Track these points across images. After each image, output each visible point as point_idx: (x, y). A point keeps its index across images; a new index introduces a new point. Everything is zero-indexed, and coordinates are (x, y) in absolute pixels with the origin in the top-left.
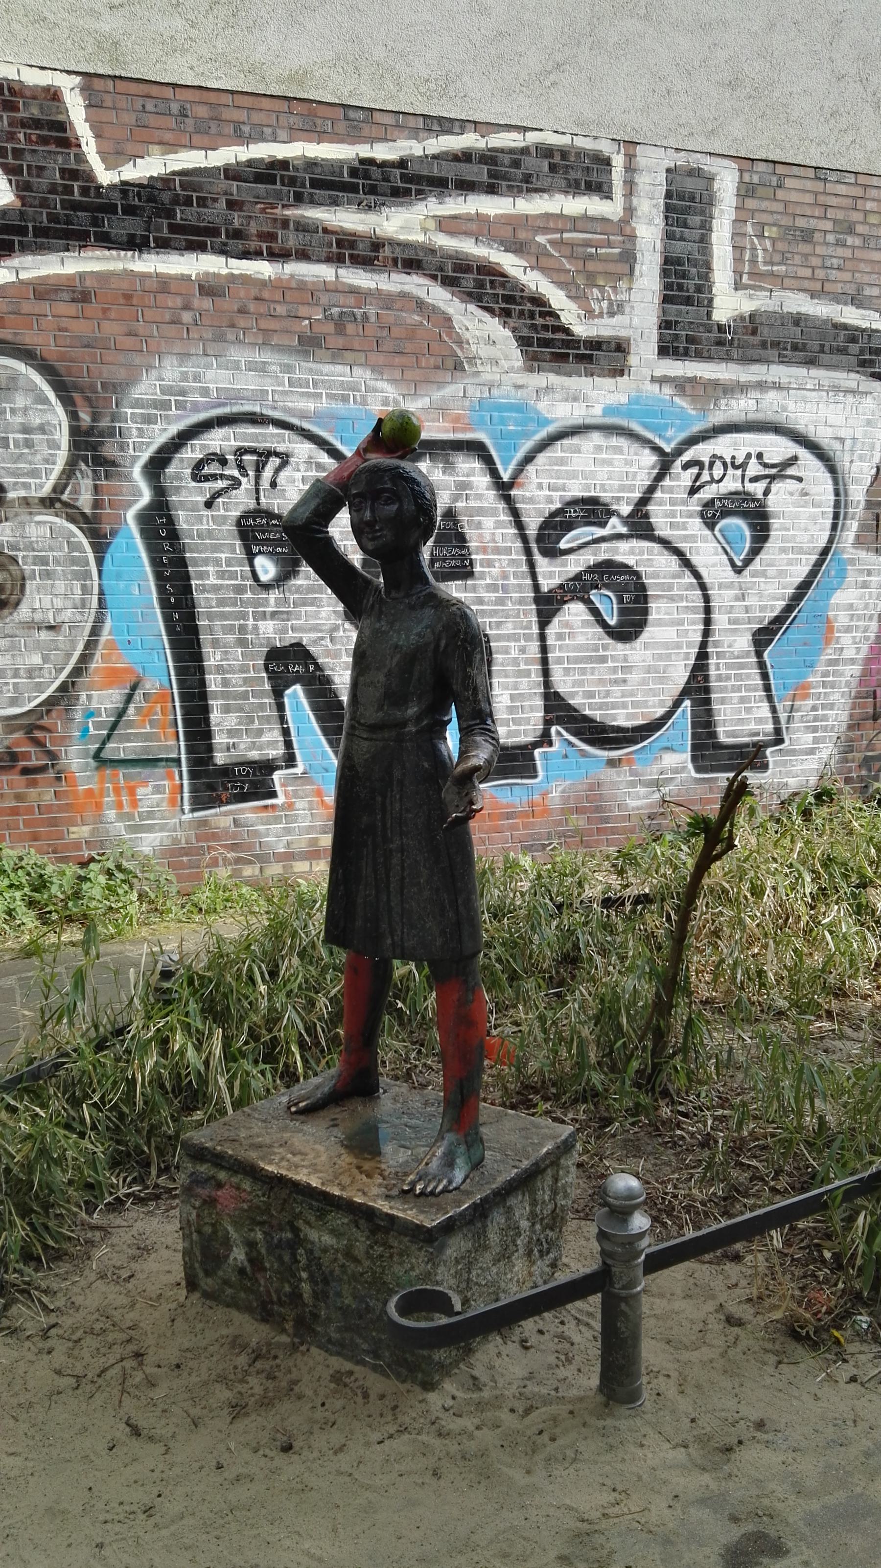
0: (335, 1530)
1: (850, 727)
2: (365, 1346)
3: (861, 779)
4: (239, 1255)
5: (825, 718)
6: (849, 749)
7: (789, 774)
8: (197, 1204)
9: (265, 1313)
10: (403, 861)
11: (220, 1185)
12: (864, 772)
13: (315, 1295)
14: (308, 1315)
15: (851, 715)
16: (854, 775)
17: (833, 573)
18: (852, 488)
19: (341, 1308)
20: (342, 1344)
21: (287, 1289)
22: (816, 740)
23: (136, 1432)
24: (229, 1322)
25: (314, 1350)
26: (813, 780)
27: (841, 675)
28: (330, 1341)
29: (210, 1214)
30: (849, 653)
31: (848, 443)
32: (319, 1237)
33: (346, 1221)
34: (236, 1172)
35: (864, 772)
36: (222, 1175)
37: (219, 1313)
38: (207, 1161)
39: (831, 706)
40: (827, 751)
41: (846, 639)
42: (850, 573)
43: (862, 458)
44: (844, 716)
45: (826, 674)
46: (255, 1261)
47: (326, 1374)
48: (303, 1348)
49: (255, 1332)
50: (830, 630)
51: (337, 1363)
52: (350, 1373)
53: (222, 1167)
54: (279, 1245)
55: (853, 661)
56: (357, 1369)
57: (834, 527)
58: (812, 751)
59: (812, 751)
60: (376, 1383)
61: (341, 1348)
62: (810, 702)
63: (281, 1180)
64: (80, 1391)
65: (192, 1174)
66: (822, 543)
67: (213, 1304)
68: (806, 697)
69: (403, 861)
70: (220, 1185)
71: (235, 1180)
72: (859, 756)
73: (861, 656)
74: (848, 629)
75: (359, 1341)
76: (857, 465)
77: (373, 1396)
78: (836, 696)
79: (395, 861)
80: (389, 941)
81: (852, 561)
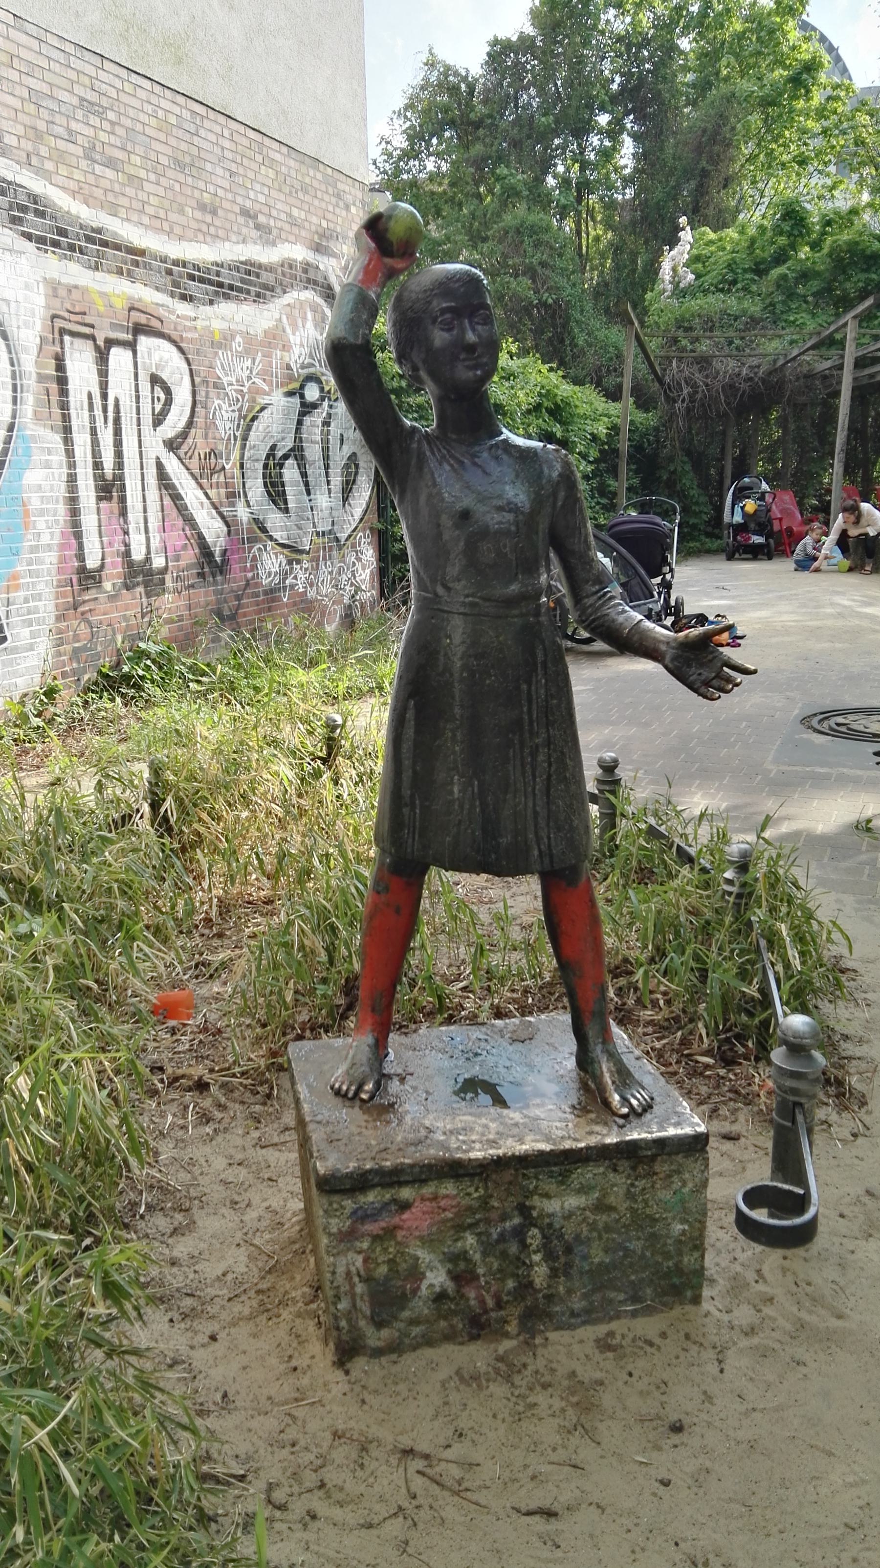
0: (830, 1454)
1: (58, 619)
2: (622, 1297)
3: (74, 672)
4: (437, 1278)
5: (36, 610)
6: (60, 643)
7: (16, 674)
8: (365, 1245)
9: (479, 1327)
10: (549, 756)
11: (405, 1206)
12: (75, 665)
13: (554, 1274)
14: (541, 1301)
15: (57, 605)
16: (67, 669)
17: (20, 451)
18: (23, 357)
19: (590, 1271)
20: (588, 1311)
21: (511, 1284)
22: (33, 635)
23: (549, 1514)
24: (433, 1366)
25: (553, 1336)
26: (37, 679)
27: (42, 563)
28: (573, 1314)
29: (385, 1250)
30: (45, 539)
31: (13, 305)
32: (560, 1204)
33: (602, 1170)
34: (424, 1182)
35: (75, 665)
36: (406, 1193)
37: (411, 1362)
38: (374, 1186)
39: (38, 597)
40: (44, 645)
41: (41, 523)
42: (35, 451)
43: (27, 325)
44: (51, 607)
45: (30, 564)
46: (463, 1276)
47: (590, 1348)
48: (538, 1341)
49: (478, 1355)
50: (27, 513)
51: (590, 1332)
52: (611, 1334)
53: (401, 1184)
54: (502, 1238)
55: (49, 547)
56: (614, 1325)
57: (15, 401)
58: (31, 647)
59: (31, 647)
60: (648, 1326)
61: (588, 1316)
62: (21, 594)
63: (500, 1163)
64: (421, 1526)
65: (354, 1212)
66: (8, 419)
67: (394, 1357)
68: (17, 588)
69: (549, 756)
70: (405, 1206)
71: (428, 1190)
72: (67, 648)
73: (56, 542)
74: (41, 513)
75: (612, 1295)
76: (23, 331)
77: (657, 1341)
78: (41, 586)
79: (541, 758)
80: (536, 853)
81: (34, 439)
